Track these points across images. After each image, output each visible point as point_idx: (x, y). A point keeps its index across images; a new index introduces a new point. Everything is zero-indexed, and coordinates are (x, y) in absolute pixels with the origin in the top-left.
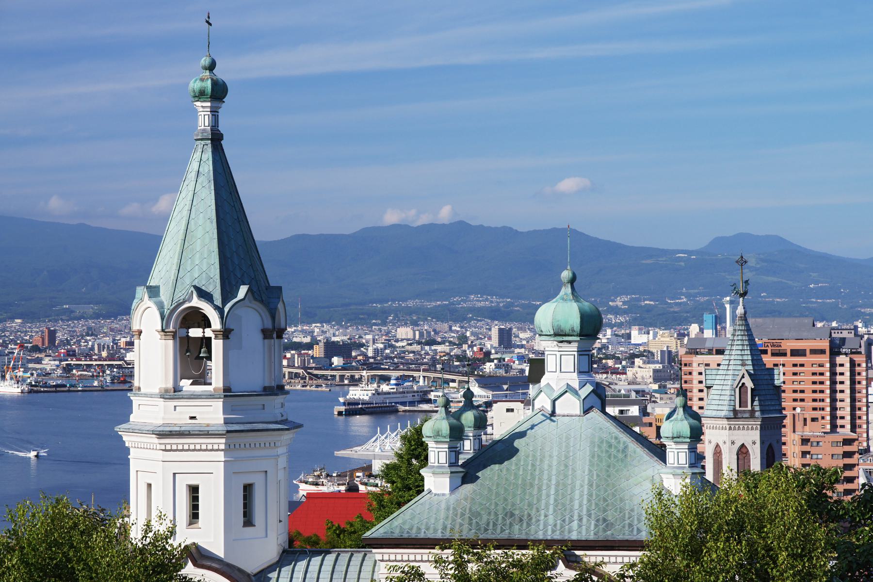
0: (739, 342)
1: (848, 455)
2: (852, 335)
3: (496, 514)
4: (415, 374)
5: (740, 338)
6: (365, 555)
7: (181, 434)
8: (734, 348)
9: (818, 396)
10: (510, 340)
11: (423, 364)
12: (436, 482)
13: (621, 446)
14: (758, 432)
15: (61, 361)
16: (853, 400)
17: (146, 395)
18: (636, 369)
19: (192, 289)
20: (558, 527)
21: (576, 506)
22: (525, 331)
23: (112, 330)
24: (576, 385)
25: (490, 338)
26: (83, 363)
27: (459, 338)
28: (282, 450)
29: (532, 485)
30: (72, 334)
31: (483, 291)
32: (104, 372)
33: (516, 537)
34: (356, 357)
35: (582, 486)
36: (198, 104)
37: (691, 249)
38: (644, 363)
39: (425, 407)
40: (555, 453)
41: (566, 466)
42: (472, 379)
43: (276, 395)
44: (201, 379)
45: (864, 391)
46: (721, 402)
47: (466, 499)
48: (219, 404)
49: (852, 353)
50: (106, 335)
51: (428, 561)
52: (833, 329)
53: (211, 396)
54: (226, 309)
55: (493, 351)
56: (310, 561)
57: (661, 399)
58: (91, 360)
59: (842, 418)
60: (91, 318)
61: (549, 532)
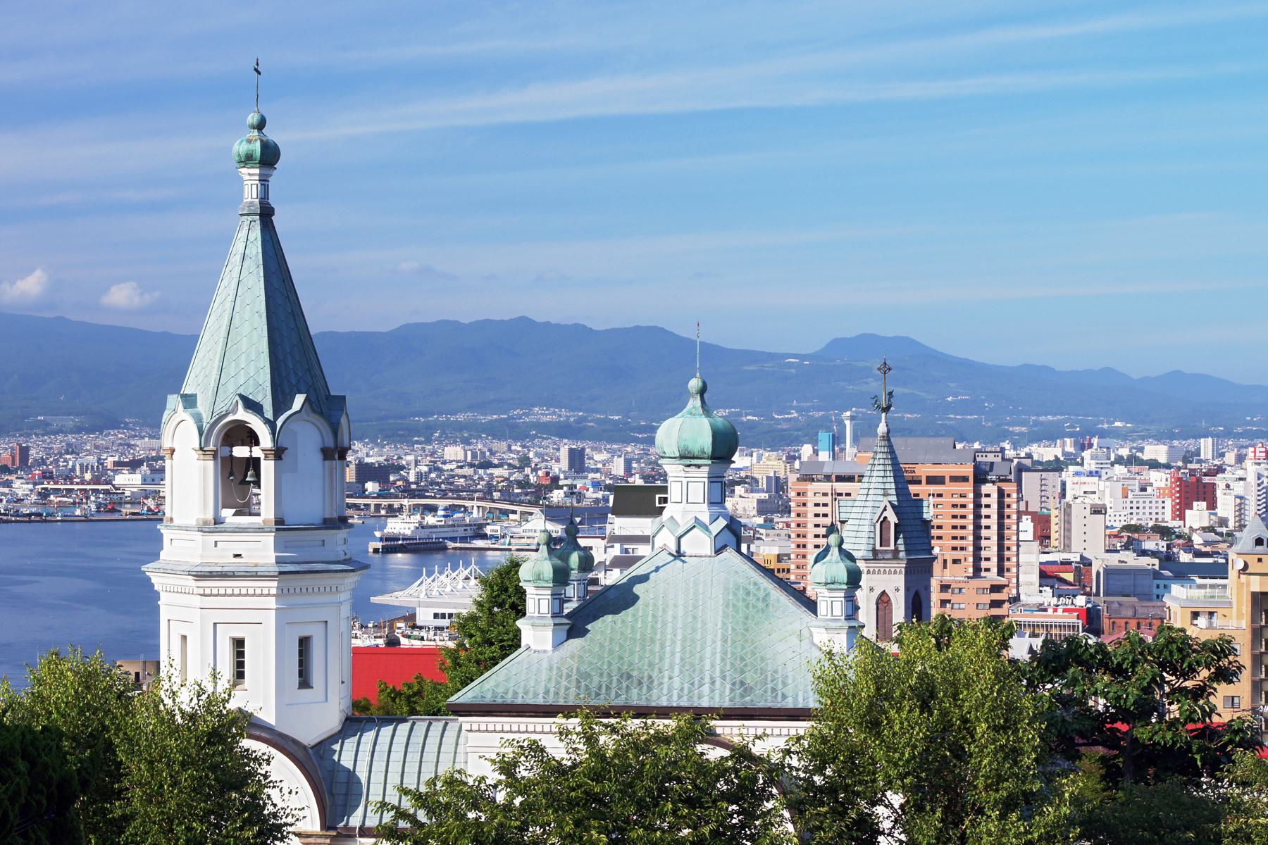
0: (881, 467)
1: (996, 604)
2: (999, 459)
3: (610, 675)
4: (468, 504)
5: (881, 461)
6: (446, 724)
7: (223, 576)
8: (875, 474)
9: (959, 532)
10: (583, 462)
11: (476, 491)
12: (536, 632)
13: (761, 594)
14: (903, 576)
15: (35, 484)
16: (1001, 537)
17: (180, 528)
18: (736, 498)
19: (237, 398)
20: (686, 691)
21: (707, 666)
22: (600, 452)
23: (96, 447)
24: (706, 519)
25: (558, 460)
26: (62, 487)
27: (520, 460)
28: (345, 596)
29: (652, 641)
30: (48, 451)
31: (549, 403)
32: (88, 498)
33: (635, 703)
34: (395, 482)
35: (714, 642)
36: (244, 171)
37: (803, 352)
38: (746, 491)
39: (479, 543)
40: (681, 602)
41: (695, 618)
42: (536, 510)
43: (339, 528)
44: (245, 509)
45: (1015, 527)
46: (857, 540)
47: (572, 657)
48: (269, 539)
49: (1001, 481)
50: (89, 453)
51: (550, 732)
52: (978, 451)
53: (260, 530)
54: (279, 423)
55: (562, 476)
56: (378, 731)
57: (767, 535)
58: (72, 484)
59: (988, 559)
60: (71, 433)
61: (675, 698)
